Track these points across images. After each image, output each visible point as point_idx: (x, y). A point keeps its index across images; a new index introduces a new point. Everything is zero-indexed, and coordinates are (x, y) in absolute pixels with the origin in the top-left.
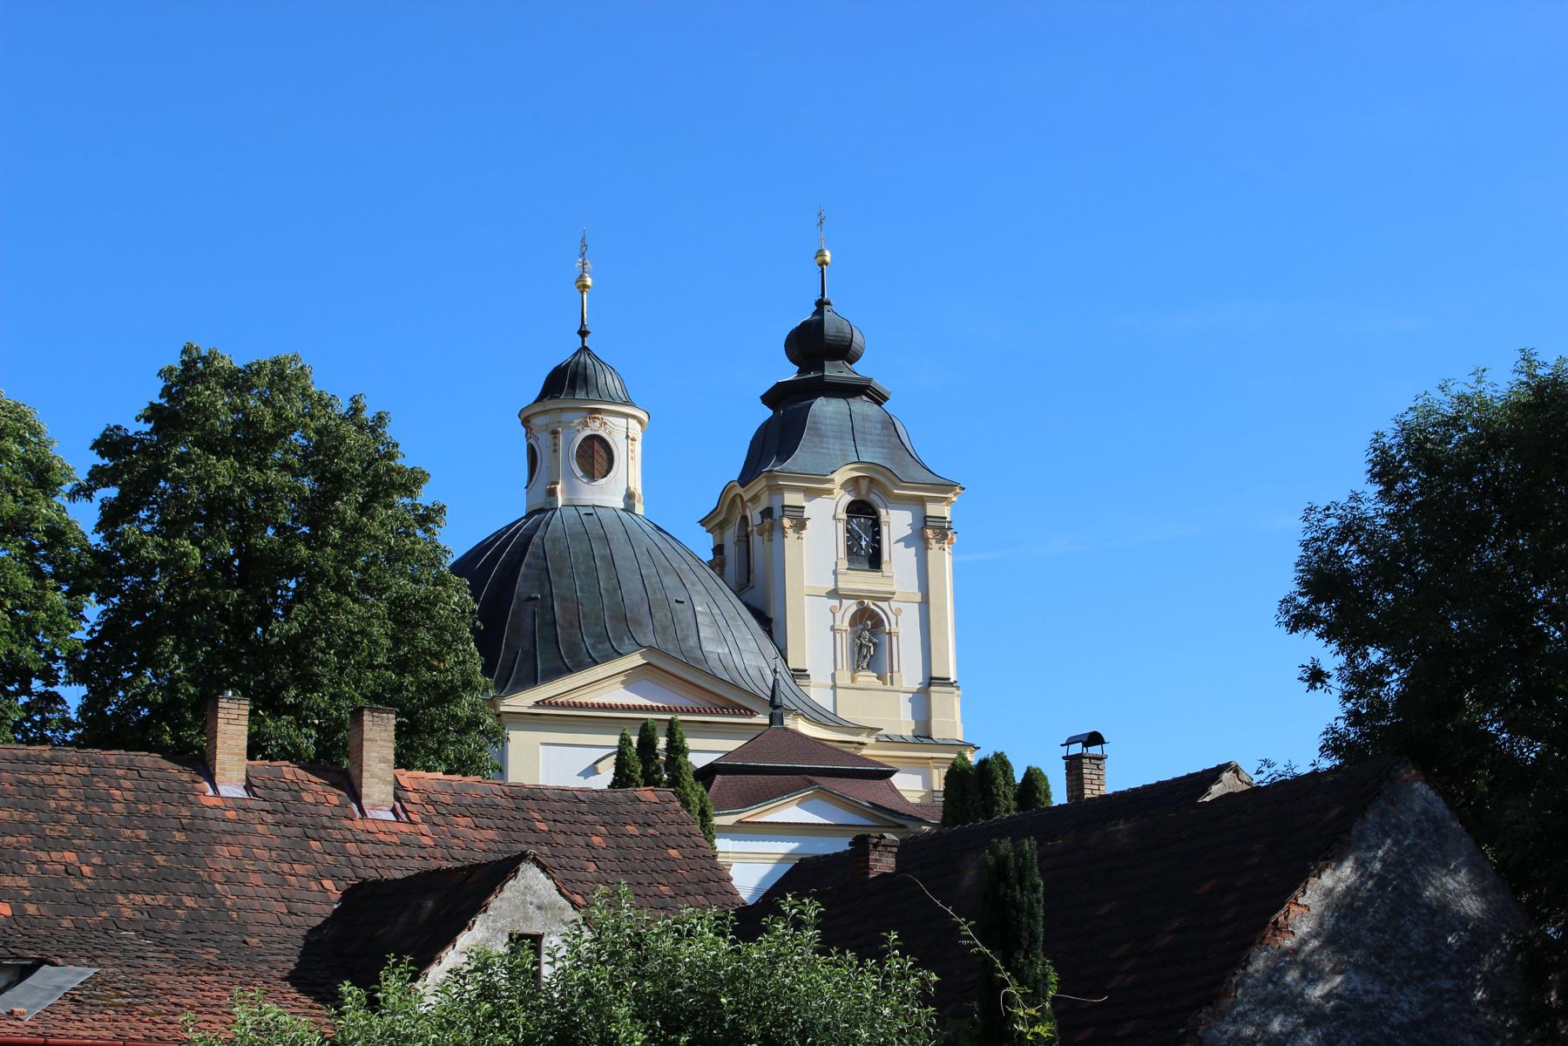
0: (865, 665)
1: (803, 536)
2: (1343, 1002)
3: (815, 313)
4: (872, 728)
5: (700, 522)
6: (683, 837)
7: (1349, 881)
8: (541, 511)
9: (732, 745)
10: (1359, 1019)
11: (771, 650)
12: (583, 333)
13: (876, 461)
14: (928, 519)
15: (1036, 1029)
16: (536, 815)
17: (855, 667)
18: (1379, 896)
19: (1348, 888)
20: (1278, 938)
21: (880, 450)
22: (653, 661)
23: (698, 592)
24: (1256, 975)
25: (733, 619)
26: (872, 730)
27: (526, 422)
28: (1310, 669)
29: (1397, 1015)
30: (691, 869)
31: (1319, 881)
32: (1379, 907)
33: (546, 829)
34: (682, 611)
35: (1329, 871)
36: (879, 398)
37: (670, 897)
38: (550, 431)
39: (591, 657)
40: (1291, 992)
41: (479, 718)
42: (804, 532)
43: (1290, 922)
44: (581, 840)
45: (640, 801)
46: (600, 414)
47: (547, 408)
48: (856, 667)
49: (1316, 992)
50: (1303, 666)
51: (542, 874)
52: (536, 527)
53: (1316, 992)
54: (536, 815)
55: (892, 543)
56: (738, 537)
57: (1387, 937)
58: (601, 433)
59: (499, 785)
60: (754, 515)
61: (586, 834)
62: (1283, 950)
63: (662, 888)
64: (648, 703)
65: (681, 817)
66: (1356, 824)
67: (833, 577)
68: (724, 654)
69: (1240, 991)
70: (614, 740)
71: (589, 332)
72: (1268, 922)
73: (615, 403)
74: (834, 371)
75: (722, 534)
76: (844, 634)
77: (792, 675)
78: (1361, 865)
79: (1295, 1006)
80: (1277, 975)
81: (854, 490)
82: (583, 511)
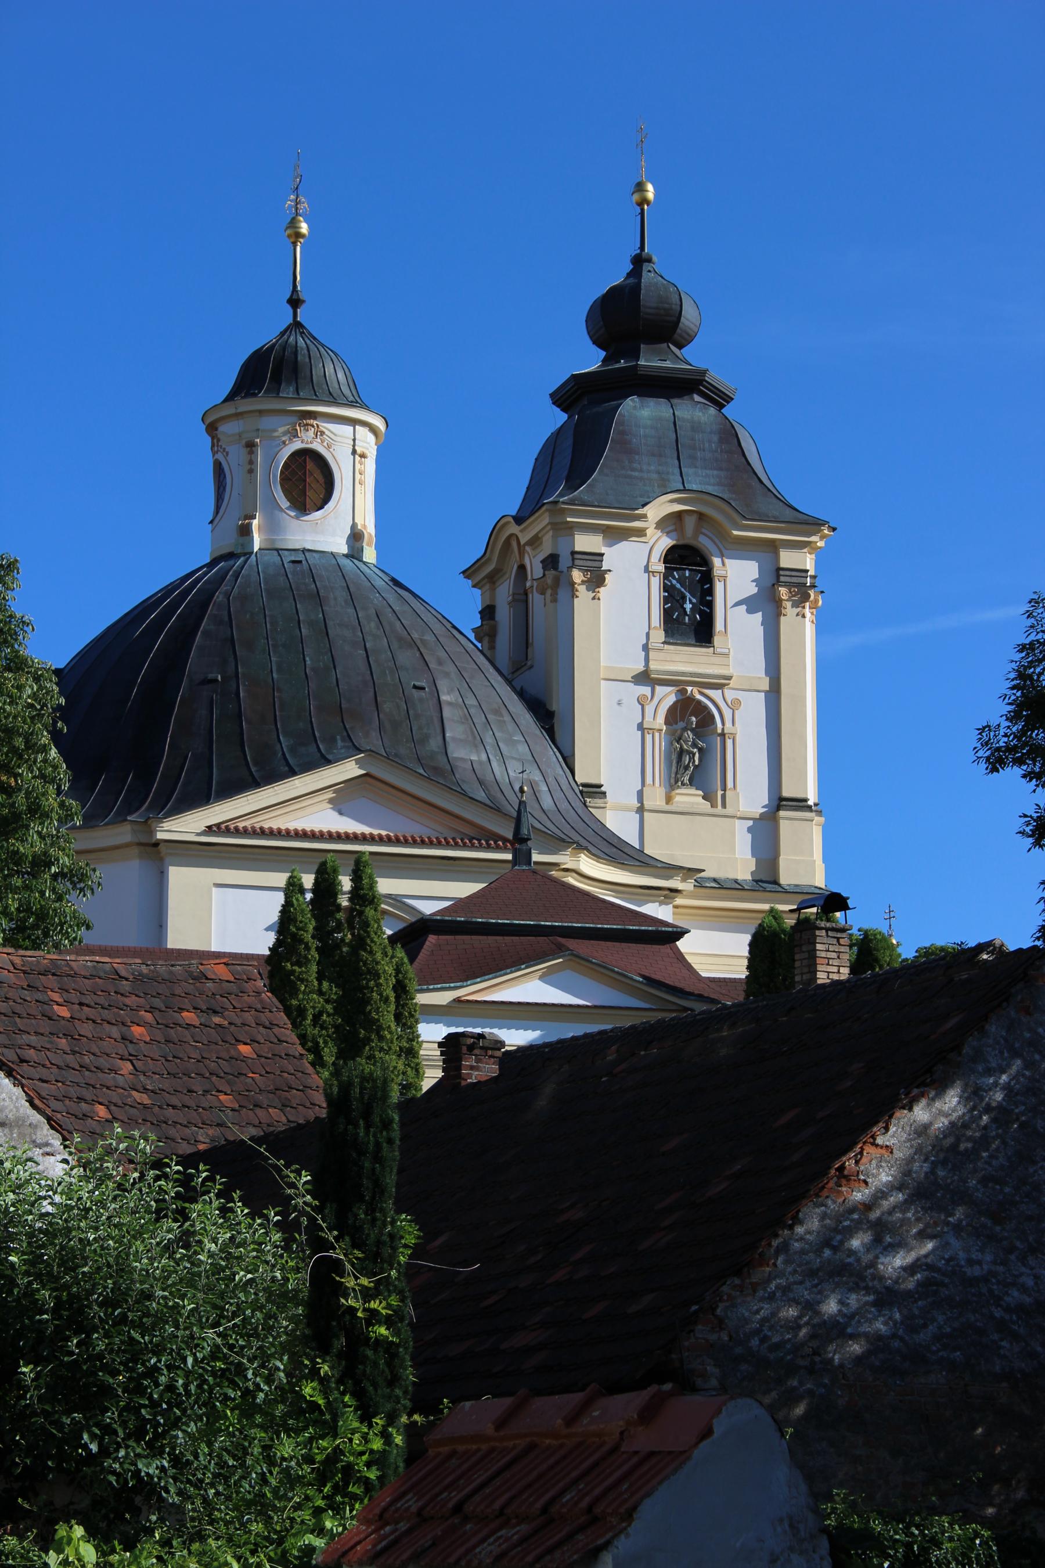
0: (686, 779)
1: (601, 595)
2: (936, 1275)
3: (629, 275)
4: (690, 869)
5: (464, 572)
6: (261, 1028)
7: (955, 1115)
8: (231, 556)
9: (465, 889)
10: (958, 1298)
11: (551, 756)
12: (295, 302)
13: (710, 489)
14: (781, 573)
15: (374, 1305)
16: (56, 997)
17: (673, 781)
18: (998, 1136)
19: (952, 1124)
20: (844, 1189)
21: (715, 472)
22: (375, 772)
23: (447, 675)
24: (808, 1236)
25: (497, 712)
26: (690, 872)
27: (212, 429)
28: (1035, 821)
29: (1016, 1294)
30: (267, 1072)
31: (909, 1114)
32: (997, 1150)
33: (67, 1015)
34: (421, 700)
35: (923, 1102)
36: (719, 399)
37: (233, 1110)
38: (244, 442)
39: (288, 764)
40: (858, 1260)
41: (50, 856)
42: (602, 590)
43: (862, 1168)
44: (115, 1032)
45: (207, 979)
46: (315, 418)
47: (240, 410)
48: (673, 783)
49: (898, 1261)
50: (1025, 816)
51: (7, 1080)
52: (221, 577)
53: (898, 1261)
54: (56, 997)
55: (729, 605)
56: (514, 594)
57: (1007, 1190)
58: (317, 446)
59: (8, 954)
60: (535, 568)
61: (123, 1024)
62: (849, 1204)
63: (222, 1097)
64: (367, 830)
65: (262, 1001)
66: (970, 1039)
67: (644, 653)
68: (480, 763)
69: (780, 1259)
70: (280, 879)
71: (303, 301)
72: (830, 1168)
73: (335, 403)
74: (649, 360)
75: (493, 590)
76: (657, 735)
77: (581, 792)
78: (974, 1095)
79: (863, 1278)
80: (839, 1237)
81: (675, 530)
82: (288, 558)
